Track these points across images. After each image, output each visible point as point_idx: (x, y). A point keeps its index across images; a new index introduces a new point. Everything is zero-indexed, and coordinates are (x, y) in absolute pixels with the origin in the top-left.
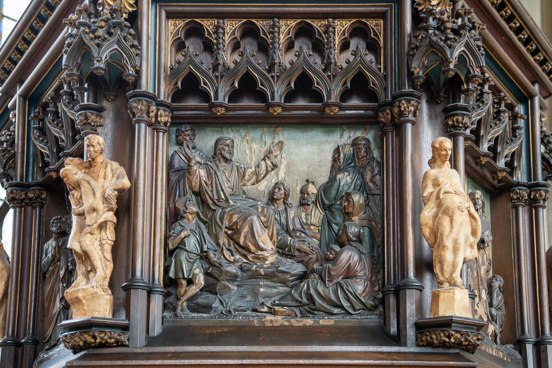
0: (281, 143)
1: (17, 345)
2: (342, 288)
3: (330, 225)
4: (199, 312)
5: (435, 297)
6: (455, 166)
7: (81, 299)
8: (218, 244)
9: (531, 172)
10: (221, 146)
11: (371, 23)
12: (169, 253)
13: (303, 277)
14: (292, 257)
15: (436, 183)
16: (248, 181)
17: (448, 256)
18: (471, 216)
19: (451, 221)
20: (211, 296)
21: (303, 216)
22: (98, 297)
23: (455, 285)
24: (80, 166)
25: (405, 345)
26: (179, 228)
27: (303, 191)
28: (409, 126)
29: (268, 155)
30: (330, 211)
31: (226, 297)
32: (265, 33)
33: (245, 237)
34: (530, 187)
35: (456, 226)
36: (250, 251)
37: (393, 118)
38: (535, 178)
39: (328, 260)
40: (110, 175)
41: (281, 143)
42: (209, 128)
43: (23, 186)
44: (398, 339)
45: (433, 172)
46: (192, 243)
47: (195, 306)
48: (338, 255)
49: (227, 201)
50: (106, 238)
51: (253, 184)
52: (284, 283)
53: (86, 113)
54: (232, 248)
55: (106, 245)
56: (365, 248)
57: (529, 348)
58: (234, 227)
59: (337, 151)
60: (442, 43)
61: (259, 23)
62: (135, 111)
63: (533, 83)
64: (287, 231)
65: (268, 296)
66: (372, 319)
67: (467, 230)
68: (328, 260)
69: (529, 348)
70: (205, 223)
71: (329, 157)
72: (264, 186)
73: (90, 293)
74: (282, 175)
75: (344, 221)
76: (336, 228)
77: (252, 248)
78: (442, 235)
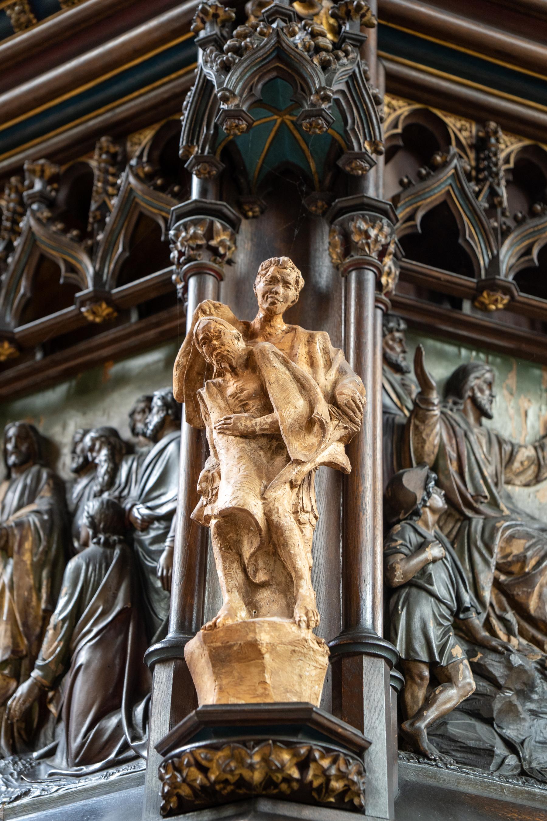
7: (264, 650)
10: (477, 382)
16: (518, 474)
22: (305, 655)
50: (309, 509)
51: (527, 485)
53: (212, 223)
55: (308, 526)
58: (515, 568)
73: (291, 638)
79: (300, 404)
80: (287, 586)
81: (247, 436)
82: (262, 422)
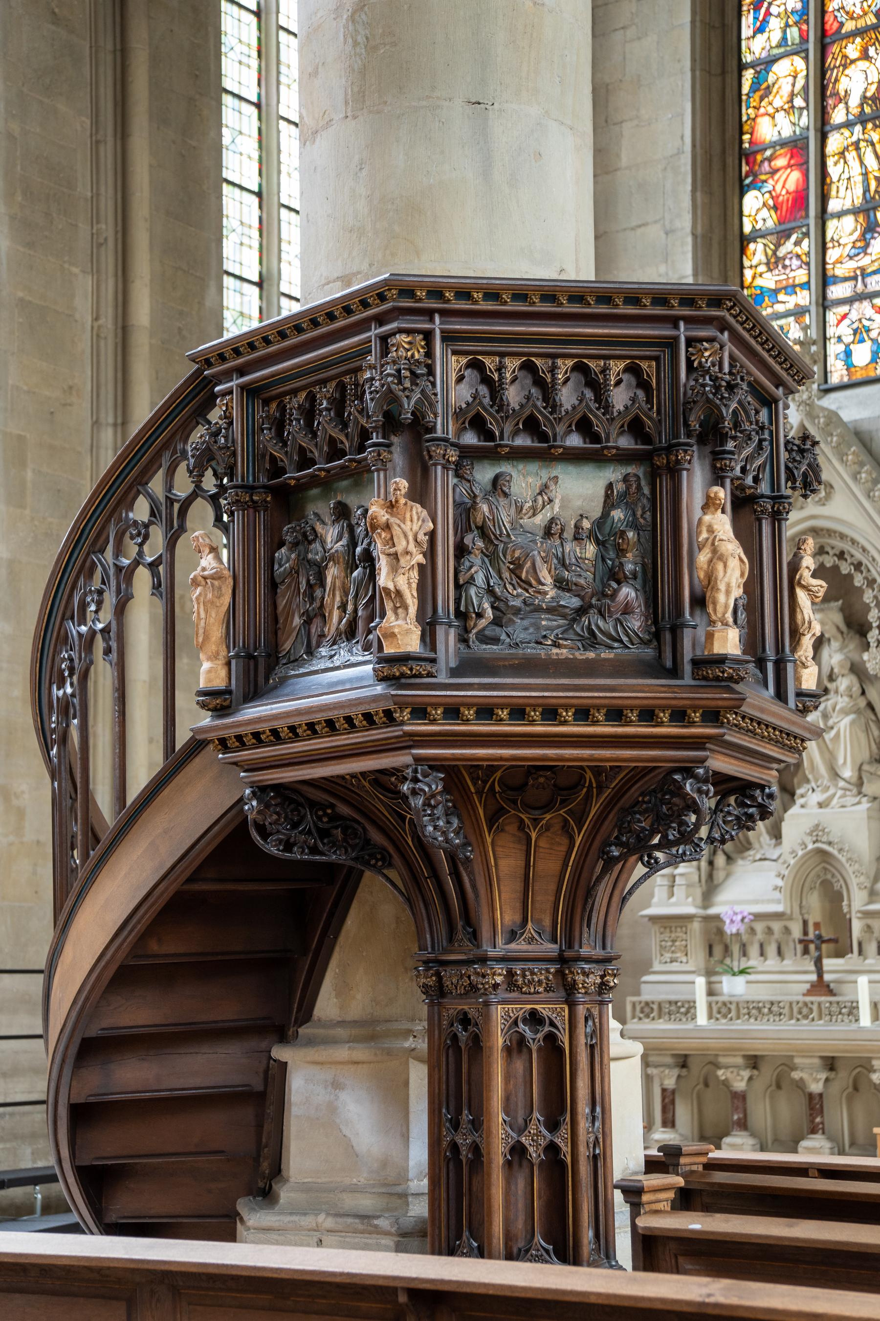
0: (557, 477)
1: (250, 657)
2: (622, 624)
3: (603, 560)
4: (487, 644)
5: (710, 636)
6: (723, 512)
8: (501, 578)
9: (774, 484)
11: (644, 365)
12: (458, 586)
13: (582, 611)
14: (569, 590)
15: (711, 530)
17: (721, 598)
18: (741, 560)
19: (725, 566)
20: (498, 629)
21: (578, 550)
23: (727, 625)
24: (828, 732)
25: (683, 678)
26: (467, 564)
27: (577, 527)
28: (685, 473)
29: (544, 489)
30: (604, 546)
31: (510, 630)
32: (543, 372)
33: (527, 572)
34: (772, 498)
35: (729, 571)
36: (531, 586)
37: (668, 462)
38: (779, 490)
39: (605, 595)
40: (415, 517)
41: (557, 477)
42: (486, 461)
43: (250, 489)
44: (675, 672)
45: (707, 518)
46: (480, 579)
47: (483, 638)
48: (615, 592)
49: (508, 535)
52: (564, 616)
54: (514, 582)
56: (638, 584)
57: (770, 666)
59: (610, 486)
60: (718, 402)
61: (538, 362)
62: (433, 454)
63: (777, 387)
64: (564, 565)
65: (551, 629)
66: (649, 652)
67: (737, 573)
68: (605, 595)
69: (770, 666)
70: (487, 556)
71: (602, 492)
72: (540, 520)
74: (557, 509)
75: (618, 556)
76: (610, 562)
77: (533, 582)
78: (716, 579)
79: (404, 543)
80: (406, 608)
81: (389, 555)
82: (392, 550)
